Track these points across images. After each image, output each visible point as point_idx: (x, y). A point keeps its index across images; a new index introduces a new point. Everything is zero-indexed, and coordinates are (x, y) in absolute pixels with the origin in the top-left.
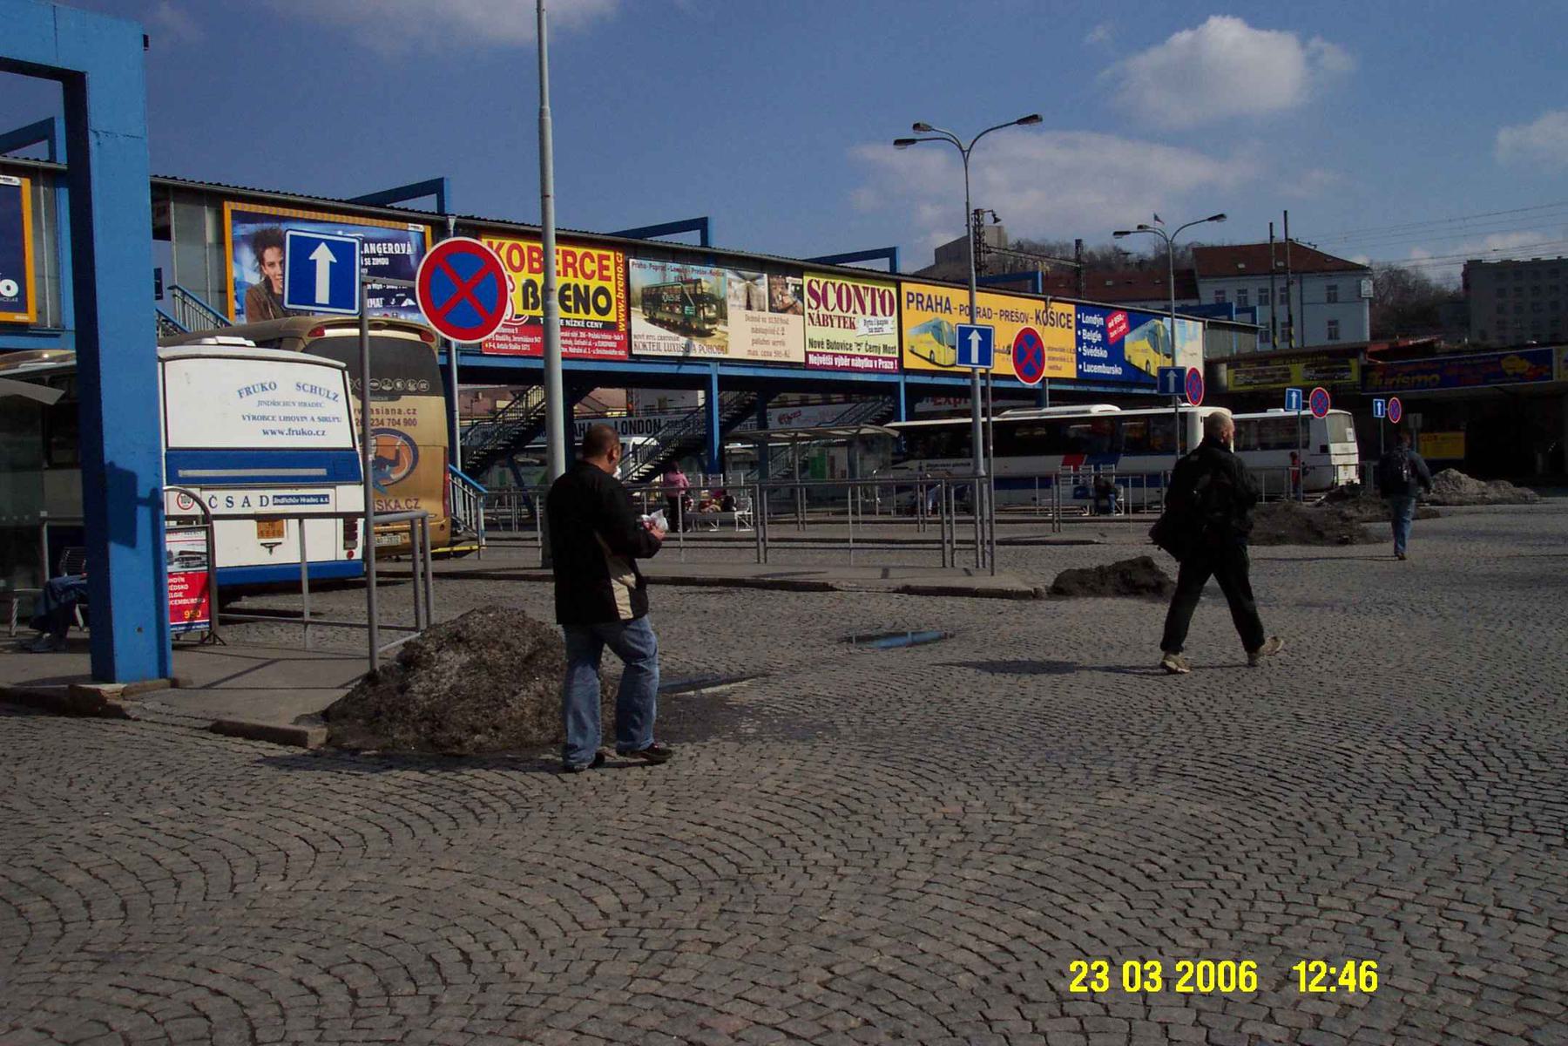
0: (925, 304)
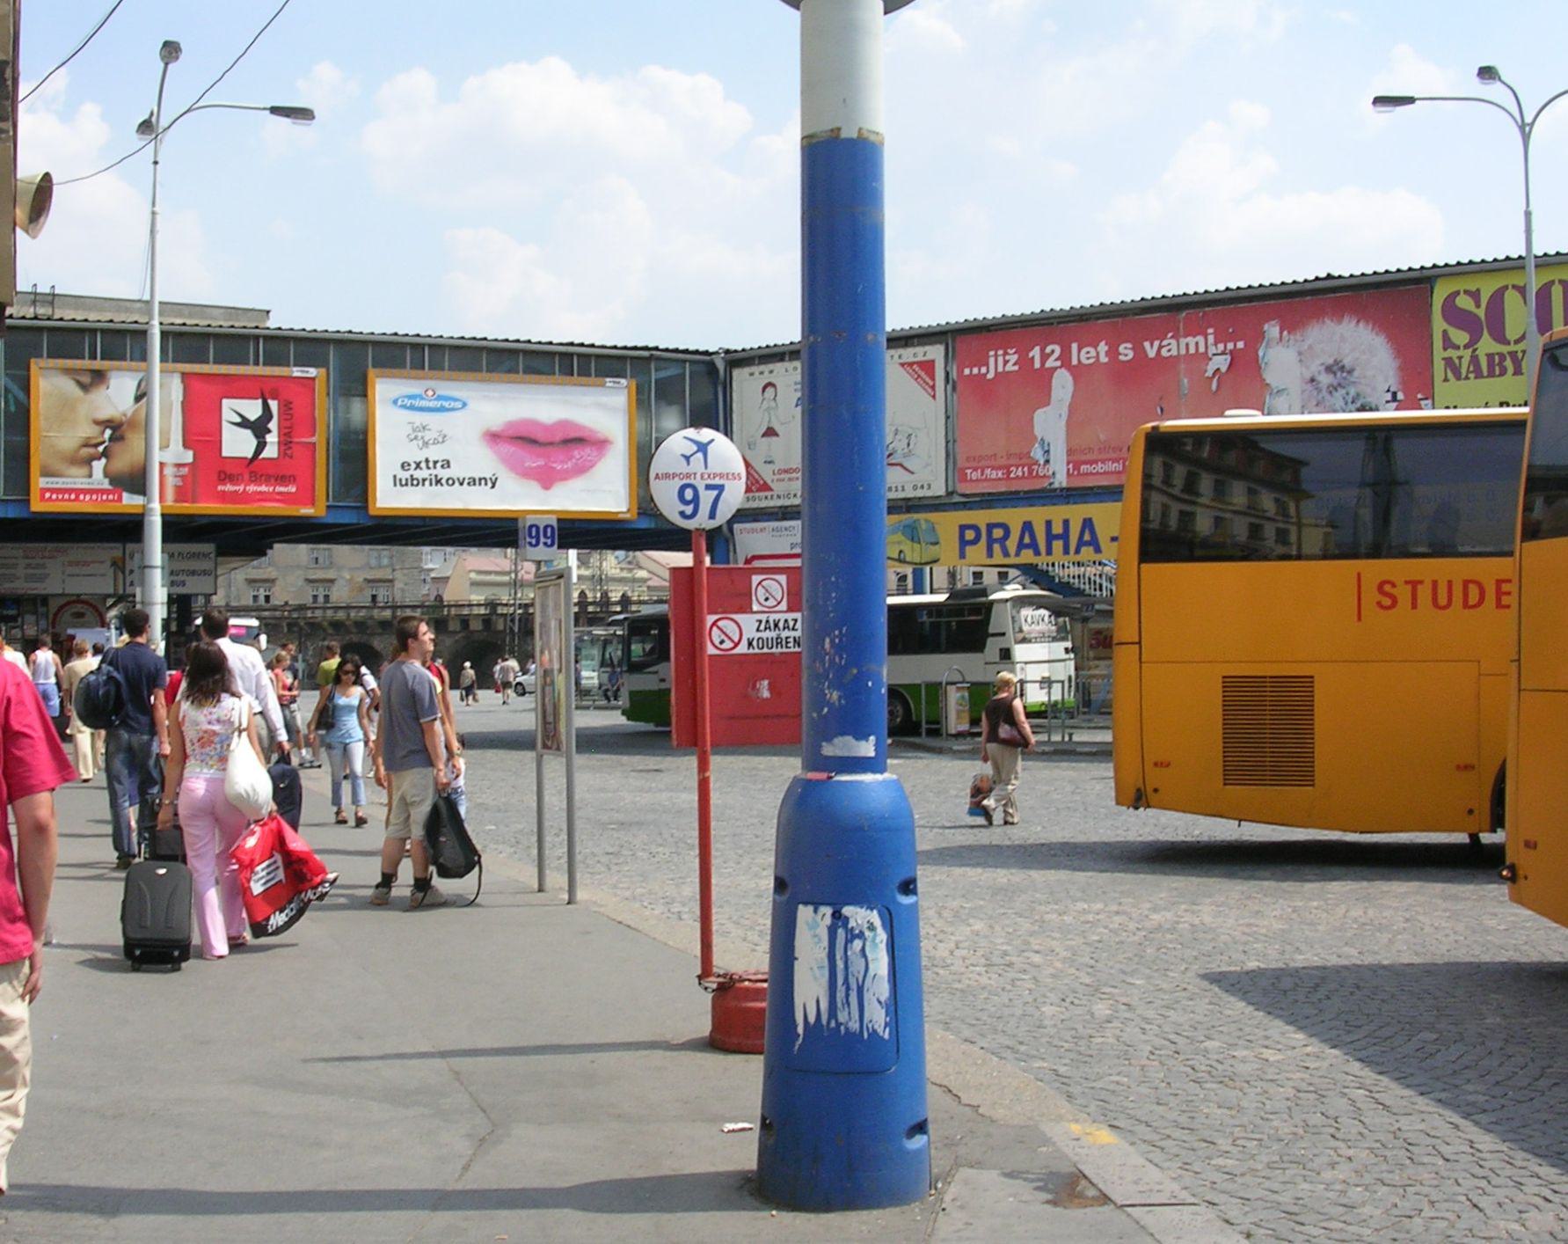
0: (1012, 544)
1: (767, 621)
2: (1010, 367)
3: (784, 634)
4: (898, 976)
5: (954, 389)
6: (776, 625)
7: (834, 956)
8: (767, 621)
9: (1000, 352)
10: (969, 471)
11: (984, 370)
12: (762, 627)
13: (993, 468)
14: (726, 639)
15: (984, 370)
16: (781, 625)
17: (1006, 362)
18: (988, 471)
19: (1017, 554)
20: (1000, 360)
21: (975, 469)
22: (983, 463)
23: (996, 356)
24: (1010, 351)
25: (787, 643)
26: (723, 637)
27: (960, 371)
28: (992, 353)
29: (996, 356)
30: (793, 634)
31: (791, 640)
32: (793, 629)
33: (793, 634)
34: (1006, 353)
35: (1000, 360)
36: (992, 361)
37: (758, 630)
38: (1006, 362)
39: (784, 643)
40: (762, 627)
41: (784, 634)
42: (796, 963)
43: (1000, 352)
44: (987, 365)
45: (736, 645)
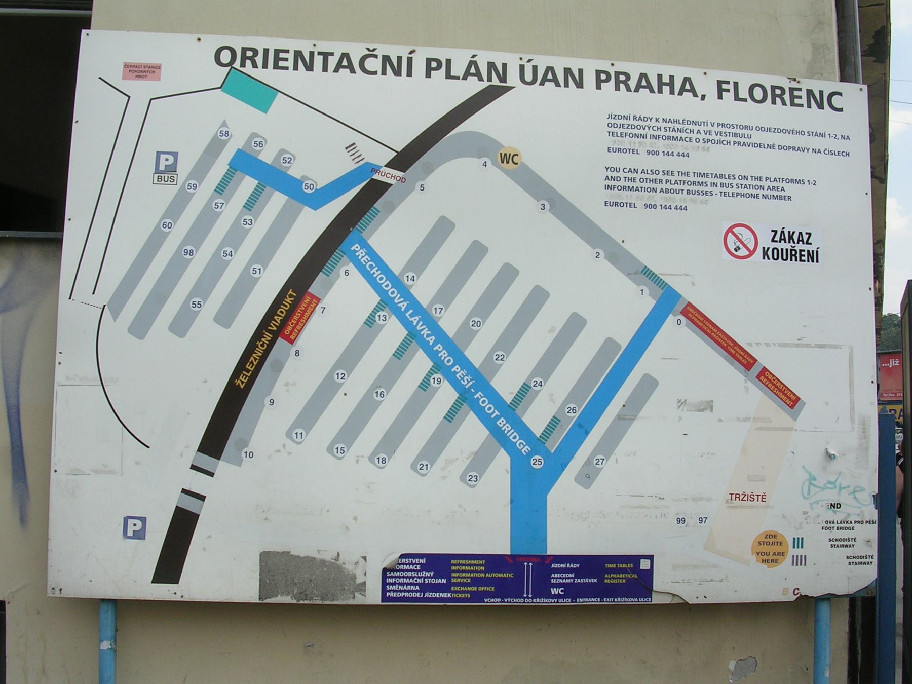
1: (782, 232)
2: (896, 364)
3: (799, 247)
4: (659, 594)
5: (879, 370)
6: (791, 237)
7: (733, 253)
8: (782, 232)
9: (894, 360)
10: (884, 394)
11: (888, 365)
12: (777, 238)
13: (892, 393)
14: (741, 246)
15: (888, 365)
16: (796, 237)
17: (895, 363)
18: (890, 394)
19: (899, 418)
20: (893, 362)
21: (886, 393)
22: (888, 392)
23: (892, 361)
24: (897, 360)
25: (801, 256)
26: (738, 244)
27: (881, 365)
28: (891, 360)
29: (892, 361)
30: (806, 247)
31: (805, 253)
32: (807, 243)
33: (806, 247)
34: (895, 360)
35: (893, 362)
36: (891, 362)
37: (773, 240)
38: (895, 363)
39: (798, 255)
40: (777, 238)
41: (799, 247)
42: (49, 541)
43: (894, 360)
44: (889, 363)
45: (752, 253)
